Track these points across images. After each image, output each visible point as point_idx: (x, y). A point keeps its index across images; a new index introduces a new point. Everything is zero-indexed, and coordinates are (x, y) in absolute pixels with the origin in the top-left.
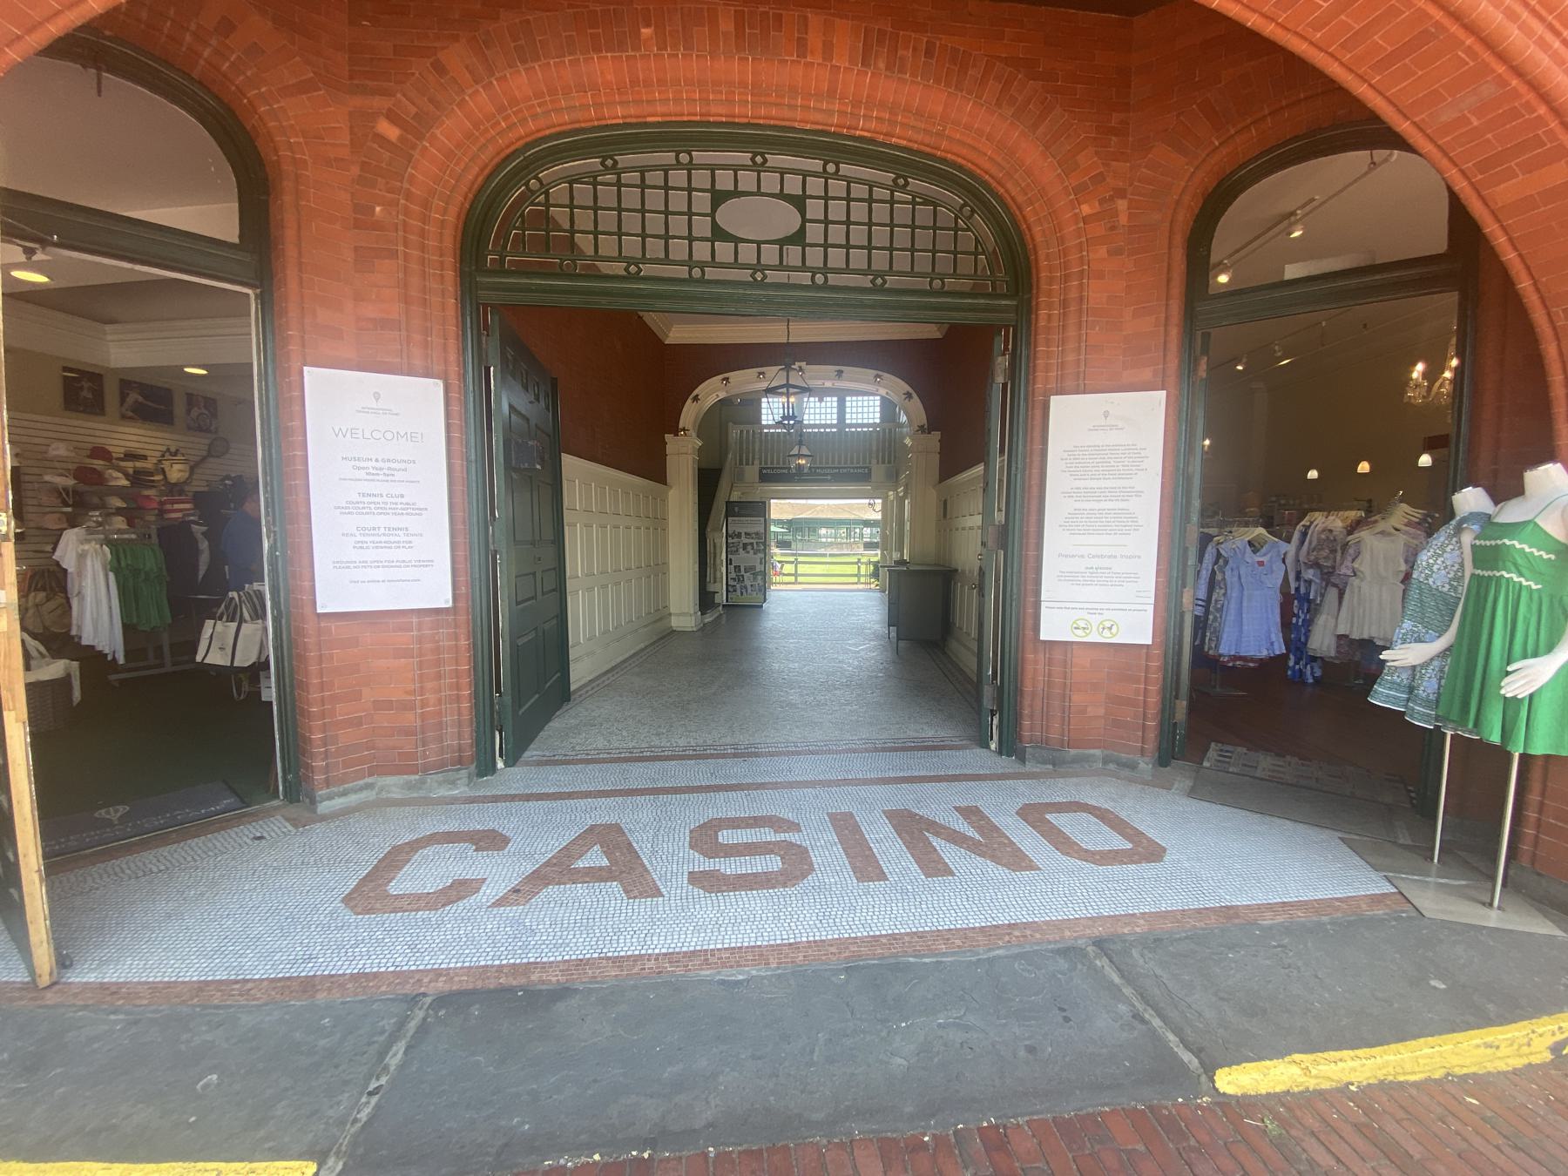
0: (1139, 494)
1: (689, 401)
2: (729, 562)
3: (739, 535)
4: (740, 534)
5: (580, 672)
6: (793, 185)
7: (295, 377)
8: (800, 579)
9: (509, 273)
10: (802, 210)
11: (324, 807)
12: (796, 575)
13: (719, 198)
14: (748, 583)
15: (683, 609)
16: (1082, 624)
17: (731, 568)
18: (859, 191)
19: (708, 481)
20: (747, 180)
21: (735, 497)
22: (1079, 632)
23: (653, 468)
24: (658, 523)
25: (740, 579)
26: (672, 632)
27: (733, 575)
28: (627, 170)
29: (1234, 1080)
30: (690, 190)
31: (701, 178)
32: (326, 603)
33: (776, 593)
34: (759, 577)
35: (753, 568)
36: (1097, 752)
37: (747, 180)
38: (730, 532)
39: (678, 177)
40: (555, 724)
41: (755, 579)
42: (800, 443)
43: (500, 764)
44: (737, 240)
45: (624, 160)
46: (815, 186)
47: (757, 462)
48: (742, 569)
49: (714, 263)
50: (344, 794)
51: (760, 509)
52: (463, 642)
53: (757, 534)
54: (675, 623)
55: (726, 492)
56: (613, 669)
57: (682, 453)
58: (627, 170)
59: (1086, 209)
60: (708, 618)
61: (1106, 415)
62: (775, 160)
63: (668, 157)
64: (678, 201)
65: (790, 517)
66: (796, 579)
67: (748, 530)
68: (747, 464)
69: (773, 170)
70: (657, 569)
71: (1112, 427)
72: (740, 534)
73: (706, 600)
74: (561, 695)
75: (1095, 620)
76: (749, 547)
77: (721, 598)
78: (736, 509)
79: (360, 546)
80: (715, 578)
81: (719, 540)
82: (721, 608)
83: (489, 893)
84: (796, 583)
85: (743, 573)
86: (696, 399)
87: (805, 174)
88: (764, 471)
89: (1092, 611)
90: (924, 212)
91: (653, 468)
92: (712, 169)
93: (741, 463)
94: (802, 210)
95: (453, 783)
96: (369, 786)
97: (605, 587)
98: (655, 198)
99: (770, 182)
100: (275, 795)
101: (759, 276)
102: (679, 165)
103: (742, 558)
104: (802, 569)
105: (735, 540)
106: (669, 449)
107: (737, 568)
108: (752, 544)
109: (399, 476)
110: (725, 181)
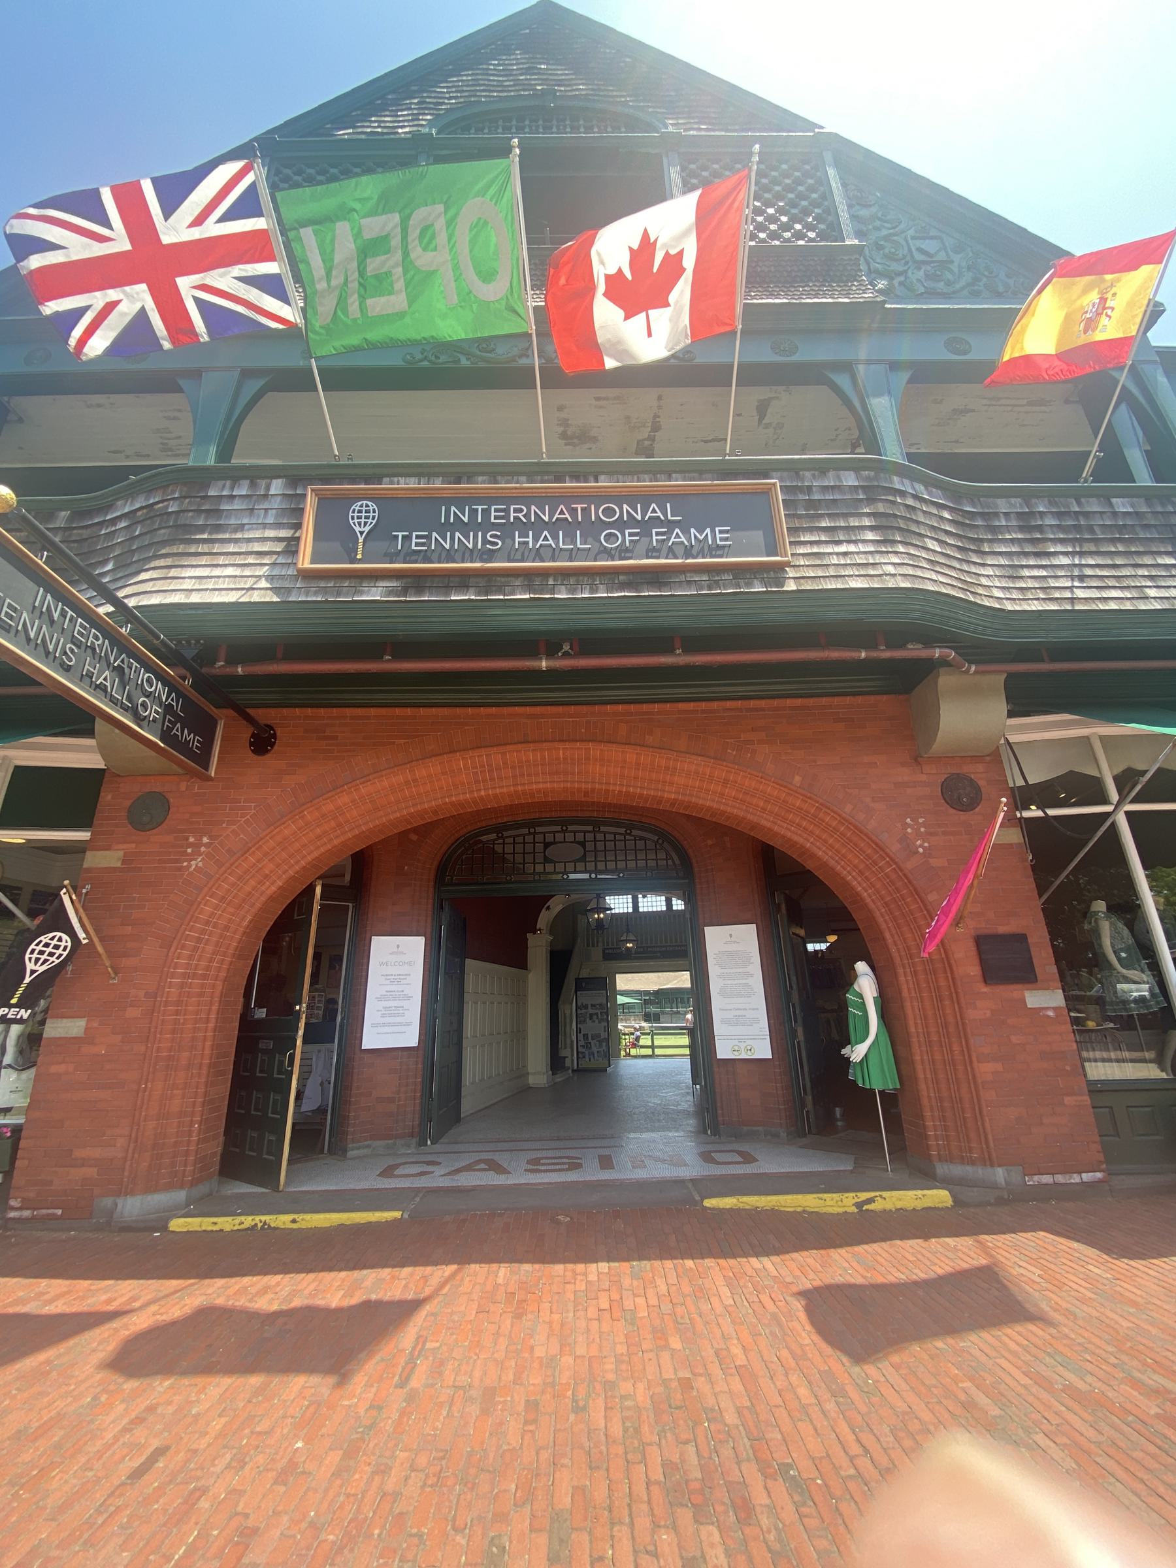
0: (752, 975)
1: (544, 910)
2: (579, 1031)
3: (586, 1007)
4: (587, 1005)
5: (468, 1105)
6: (580, 837)
7: (367, 942)
8: (658, 1051)
9: (456, 884)
10: (584, 847)
11: (350, 1154)
12: (653, 1047)
13: (547, 845)
14: (595, 1049)
15: (538, 1071)
16: (736, 1048)
17: (581, 1036)
18: (611, 837)
19: (559, 963)
20: (559, 837)
21: (584, 974)
22: (736, 1053)
23: (517, 959)
24: (520, 999)
25: (588, 1046)
26: (528, 1088)
27: (582, 1043)
28: (507, 837)
29: (708, 1203)
30: (534, 843)
31: (539, 838)
32: (752, 928)
33: (630, 1062)
34: (604, 1044)
35: (599, 1036)
36: (760, 1128)
37: (559, 837)
38: (579, 1004)
39: (529, 839)
40: (452, 1131)
41: (601, 1046)
42: (628, 931)
43: (429, 1142)
44: (555, 862)
45: (506, 834)
46: (590, 837)
47: (600, 944)
48: (590, 1038)
49: (545, 873)
50: (358, 1148)
51: (604, 985)
52: (420, 1066)
53: (600, 1005)
54: (533, 1080)
55: (578, 969)
56: (486, 1108)
57: (538, 946)
58: (507, 837)
59: (710, 842)
60: (559, 1078)
61: (731, 936)
62: (570, 828)
63: (525, 831)
64: (529, 848)
65: (656, 988)
66: (653, 1051)
67: (593, 1003)
68: (593, 946)
69: (571, 832)
70: (518, 1034)
71: (735, 942)
72: (587, 1005)
73: (556, 1063)
74: (457, 1119)
75: (742, 1045)
76: (595, 1017)
77: (571, 1061)
78: (584, 985)
79: (383, 1016)
80: (565, 1044)
81: (568, 1010)
82: (570, 1071)
83: (436, 1174)
84: (652, 1056)
85: (590, 1040)
86: (548, 908)
87: (585, 832)
88: (607, 951)
89: (740, 1041)
90: (640, 844)
91: (517, 959)
92: (544, 833)
93: (588, 946)
94: (584, 847)
95: (409, 1146)
96: (368, 1146)
97: (483, 1046)
98: (519, 848)
99: (570, 837)
100: (322, 1151)
101: (565, 877)
102: (530, 833)
103: (591, 1027)
104: (659, 1041)
105: (583, 1011)
106: (530, 943)
107: (586, 1036)
108: (597, 1014)
109: (403, 982)
110: (550, 838)
